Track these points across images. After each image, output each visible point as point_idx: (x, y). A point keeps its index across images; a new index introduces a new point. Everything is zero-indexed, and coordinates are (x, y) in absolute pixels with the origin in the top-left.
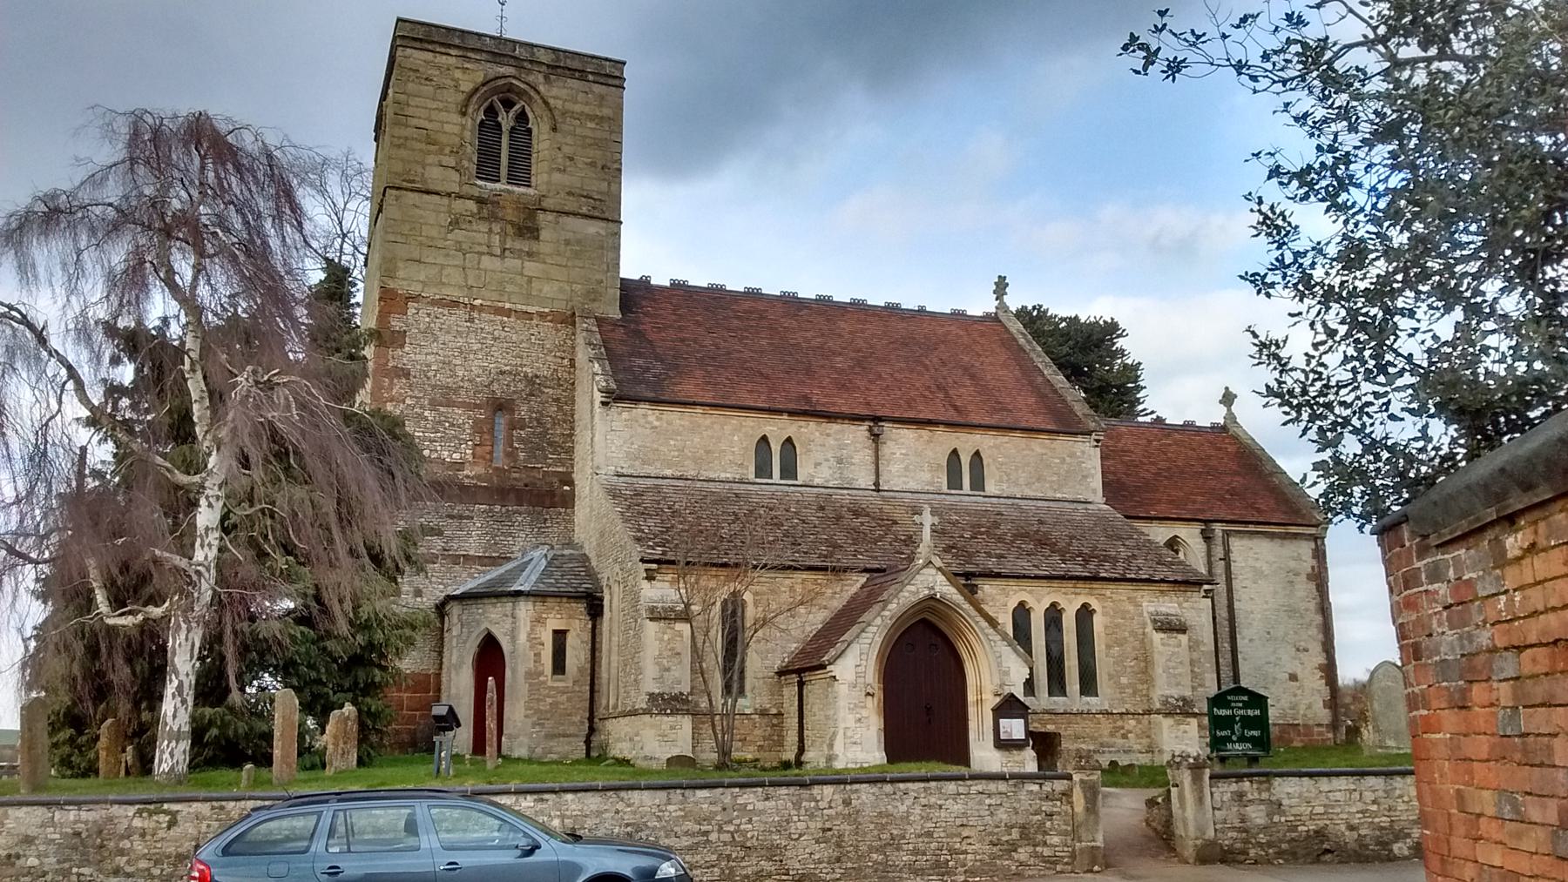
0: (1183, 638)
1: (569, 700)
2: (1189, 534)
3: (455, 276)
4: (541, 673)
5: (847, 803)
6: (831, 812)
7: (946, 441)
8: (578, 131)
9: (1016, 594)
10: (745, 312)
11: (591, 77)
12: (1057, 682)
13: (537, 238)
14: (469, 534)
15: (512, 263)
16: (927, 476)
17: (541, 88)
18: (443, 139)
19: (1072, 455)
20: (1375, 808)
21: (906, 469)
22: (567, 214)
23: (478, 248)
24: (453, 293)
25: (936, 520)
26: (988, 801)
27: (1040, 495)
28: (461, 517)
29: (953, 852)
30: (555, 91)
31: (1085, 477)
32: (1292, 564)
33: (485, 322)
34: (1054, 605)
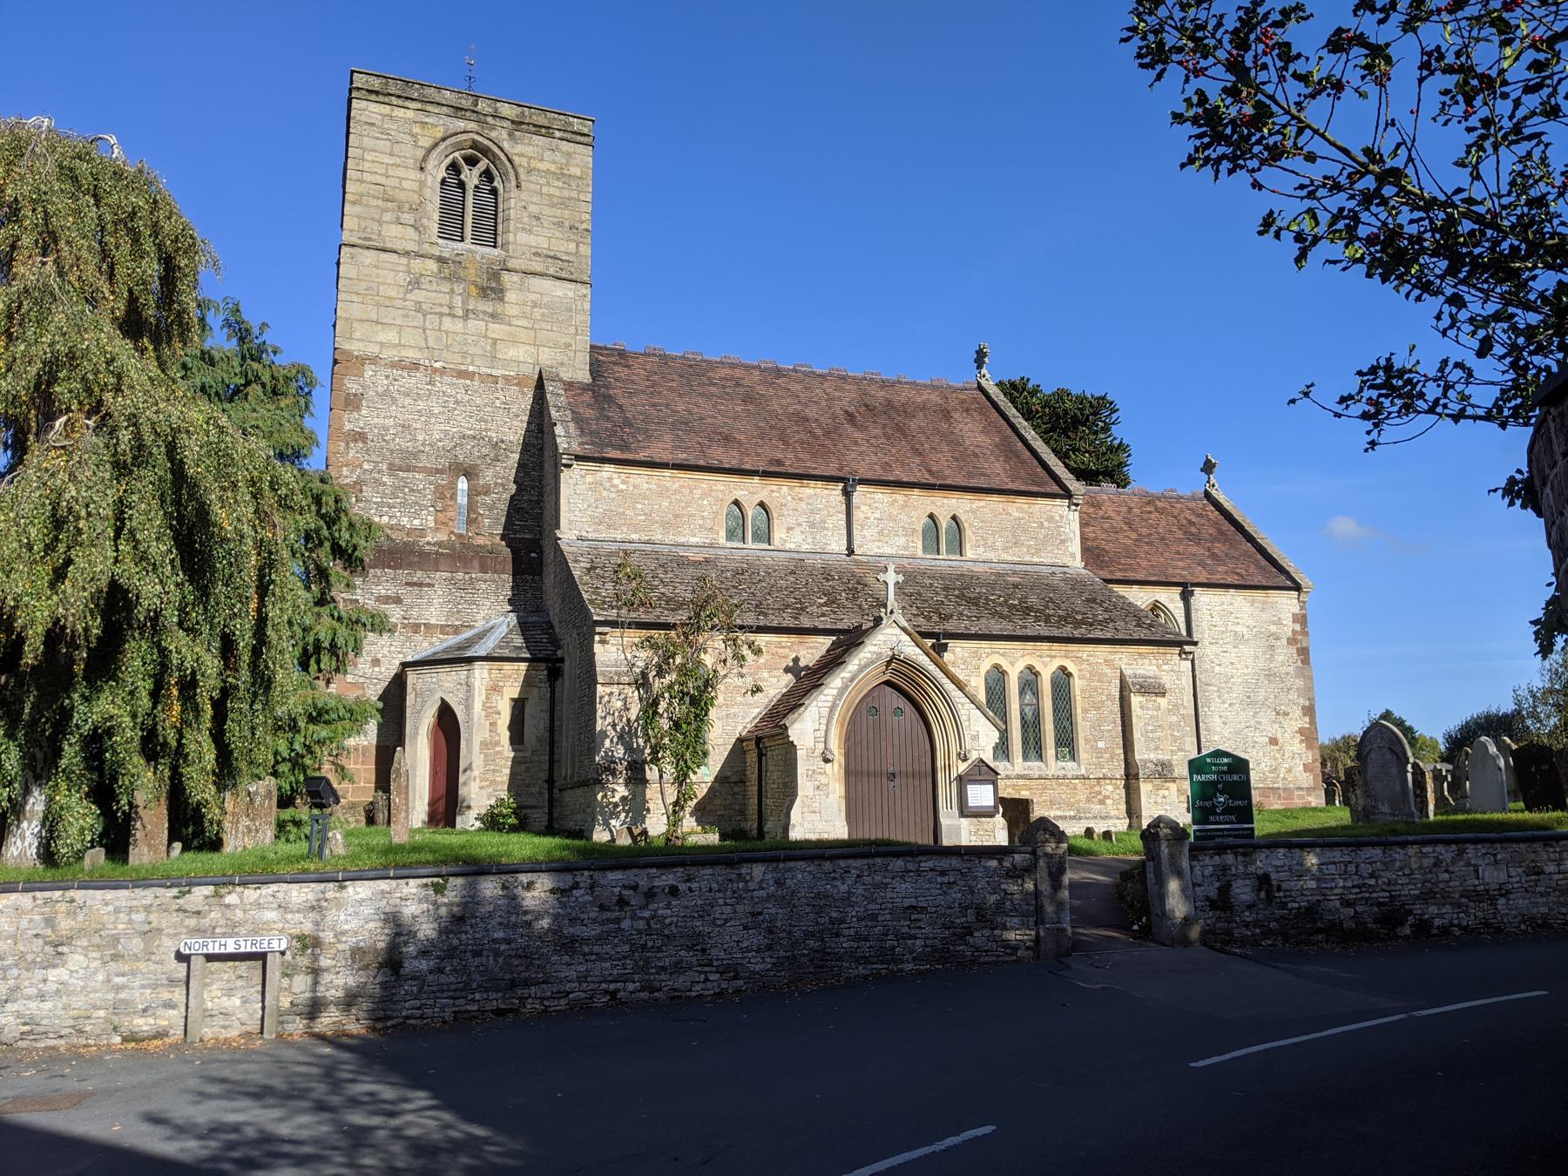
0: (1162, 701)
1: (527, 770)
2: (1170, 598)
3: (411, 337)
4: (497, 743)
5: (779, 883)
6: (763, 893)
7: (922, 504)
8: (545, 190)
9: (990, 655)
10: (721, 379)
11: (558, 134)
12: (1033, 747)
13: (501, 299)
14: (430, 603)
15: (475, 325)
16: (902, 541)
17: (506, 145)
18: (402, 196)
19: (1051, 519)
20: (1372, 882)
21: (880, 533)
22: (534, 274)
23: (439, 310)
24: (411, 354)
25: (901, 578)
26: (939, 879)
27: (1016, 559)
28: (420, 585)
29: (900, 937)
30: (519, 149)
31: (1063, 541)
32: (1273, 628)
33: (444, 384)
34: (1030, 668)
